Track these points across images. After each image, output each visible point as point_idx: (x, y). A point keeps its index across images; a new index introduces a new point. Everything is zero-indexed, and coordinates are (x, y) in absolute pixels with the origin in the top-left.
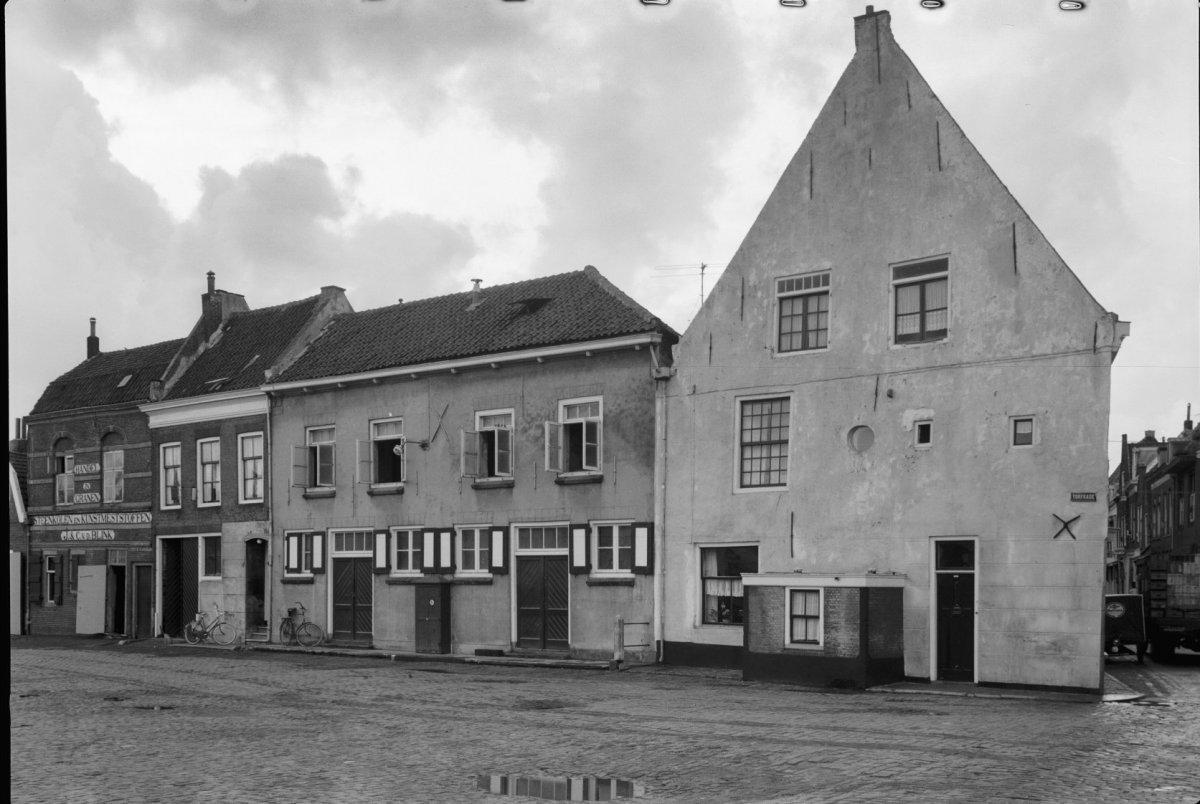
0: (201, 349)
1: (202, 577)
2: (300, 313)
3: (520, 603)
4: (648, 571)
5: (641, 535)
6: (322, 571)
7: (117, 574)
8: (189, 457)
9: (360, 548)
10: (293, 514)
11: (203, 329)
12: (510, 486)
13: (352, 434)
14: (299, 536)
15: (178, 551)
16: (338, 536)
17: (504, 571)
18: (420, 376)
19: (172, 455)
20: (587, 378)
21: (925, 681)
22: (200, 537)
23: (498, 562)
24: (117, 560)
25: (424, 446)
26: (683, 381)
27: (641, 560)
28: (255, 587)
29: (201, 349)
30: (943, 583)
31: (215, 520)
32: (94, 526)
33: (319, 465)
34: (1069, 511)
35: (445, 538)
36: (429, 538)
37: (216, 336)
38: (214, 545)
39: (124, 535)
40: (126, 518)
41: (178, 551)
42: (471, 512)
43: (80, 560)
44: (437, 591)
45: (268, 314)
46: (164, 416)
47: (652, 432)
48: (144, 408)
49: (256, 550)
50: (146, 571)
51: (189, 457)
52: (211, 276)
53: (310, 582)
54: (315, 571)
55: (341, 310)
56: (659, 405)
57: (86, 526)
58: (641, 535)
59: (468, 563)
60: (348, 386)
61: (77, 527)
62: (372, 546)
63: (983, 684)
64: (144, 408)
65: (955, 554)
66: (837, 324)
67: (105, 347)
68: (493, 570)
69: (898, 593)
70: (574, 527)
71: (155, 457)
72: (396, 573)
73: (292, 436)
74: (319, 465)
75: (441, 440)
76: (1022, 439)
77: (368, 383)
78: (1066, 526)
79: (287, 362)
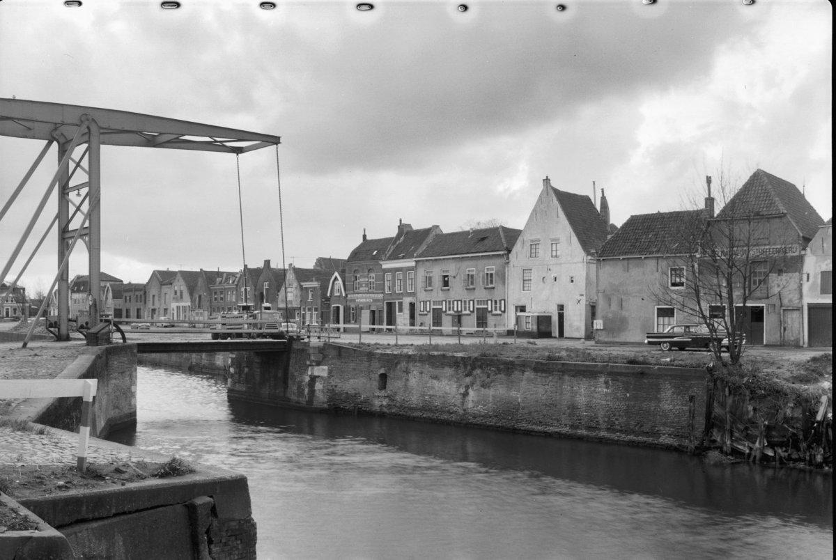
0: (397, 243)
1: (397, 313)
2: (427, 232)
3: (477, 320)
4: (504, 312)
5: (503, 302)
6: (429, 312)
7: (373, 312)
8: (394, 277)
9: (484, 304)
10: (422, 295)
11: (399, 236)
12: (474, 289)
13: (437, 272)
14: (424, 302)
15: (390, 305)
16: (434, 302)
17: (473, 312)
18: (453, 258)
19: (389, 276)
20: (491, 261)
21: (555, 337)
22: (397, 302)
23: (471, 309)
24: (373, 308)
25: (454, 277)
26: (511, 264)
27: (503, 309)
28: (412, 316)
29: (397, 243)
30: (559, 313)
31: (401, 296)
32: (366, 298)
33: (429, 281)
34: (579, 298)
35: (459, 302)
36: (456, 302)
37: (402, 239)
38: (401, 304)
39: (375, 301)
40: (376, 295)
41: (390, 305)
42: (466, 296)
43: (362, 308)
44: (457, 317)
45: (417, 232)
46: (387, 265)
47: (505, 276)
48: (381, 263)
49: (412, 306)
50: (381, 312)
51: (394, 277)
52: (401, 221)
53: (426, 315)
54: (428, 312)
55: (438, 232)
56: (507, 269)
57: (364, 298)
58: (503, 302)
59: (465, 310)
60: (436, 260)
61: (361, 298)
62: (487, 304)
63: (566, 338)
64: (381, 263)
65: (561, 307)
66: (541, 252)
67: (368, 238)
68: (471, 311)
69: (550, 317)
70: (487, 301)
71: (384, 277)
72: (448, 312)
73: (421, 273)
74: (429, 281)
75: (458, 275)
76: (572, 281)
77: (440, 259)
78: (579, 301)
79: (420, 251)
